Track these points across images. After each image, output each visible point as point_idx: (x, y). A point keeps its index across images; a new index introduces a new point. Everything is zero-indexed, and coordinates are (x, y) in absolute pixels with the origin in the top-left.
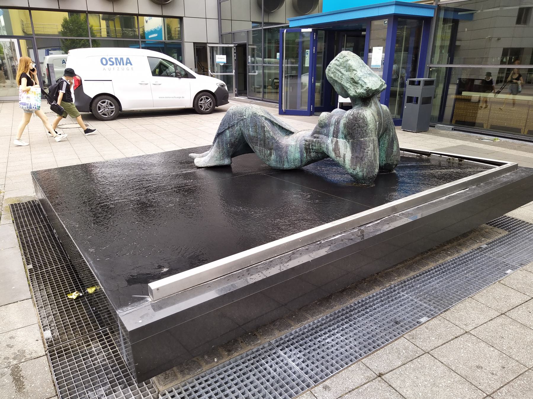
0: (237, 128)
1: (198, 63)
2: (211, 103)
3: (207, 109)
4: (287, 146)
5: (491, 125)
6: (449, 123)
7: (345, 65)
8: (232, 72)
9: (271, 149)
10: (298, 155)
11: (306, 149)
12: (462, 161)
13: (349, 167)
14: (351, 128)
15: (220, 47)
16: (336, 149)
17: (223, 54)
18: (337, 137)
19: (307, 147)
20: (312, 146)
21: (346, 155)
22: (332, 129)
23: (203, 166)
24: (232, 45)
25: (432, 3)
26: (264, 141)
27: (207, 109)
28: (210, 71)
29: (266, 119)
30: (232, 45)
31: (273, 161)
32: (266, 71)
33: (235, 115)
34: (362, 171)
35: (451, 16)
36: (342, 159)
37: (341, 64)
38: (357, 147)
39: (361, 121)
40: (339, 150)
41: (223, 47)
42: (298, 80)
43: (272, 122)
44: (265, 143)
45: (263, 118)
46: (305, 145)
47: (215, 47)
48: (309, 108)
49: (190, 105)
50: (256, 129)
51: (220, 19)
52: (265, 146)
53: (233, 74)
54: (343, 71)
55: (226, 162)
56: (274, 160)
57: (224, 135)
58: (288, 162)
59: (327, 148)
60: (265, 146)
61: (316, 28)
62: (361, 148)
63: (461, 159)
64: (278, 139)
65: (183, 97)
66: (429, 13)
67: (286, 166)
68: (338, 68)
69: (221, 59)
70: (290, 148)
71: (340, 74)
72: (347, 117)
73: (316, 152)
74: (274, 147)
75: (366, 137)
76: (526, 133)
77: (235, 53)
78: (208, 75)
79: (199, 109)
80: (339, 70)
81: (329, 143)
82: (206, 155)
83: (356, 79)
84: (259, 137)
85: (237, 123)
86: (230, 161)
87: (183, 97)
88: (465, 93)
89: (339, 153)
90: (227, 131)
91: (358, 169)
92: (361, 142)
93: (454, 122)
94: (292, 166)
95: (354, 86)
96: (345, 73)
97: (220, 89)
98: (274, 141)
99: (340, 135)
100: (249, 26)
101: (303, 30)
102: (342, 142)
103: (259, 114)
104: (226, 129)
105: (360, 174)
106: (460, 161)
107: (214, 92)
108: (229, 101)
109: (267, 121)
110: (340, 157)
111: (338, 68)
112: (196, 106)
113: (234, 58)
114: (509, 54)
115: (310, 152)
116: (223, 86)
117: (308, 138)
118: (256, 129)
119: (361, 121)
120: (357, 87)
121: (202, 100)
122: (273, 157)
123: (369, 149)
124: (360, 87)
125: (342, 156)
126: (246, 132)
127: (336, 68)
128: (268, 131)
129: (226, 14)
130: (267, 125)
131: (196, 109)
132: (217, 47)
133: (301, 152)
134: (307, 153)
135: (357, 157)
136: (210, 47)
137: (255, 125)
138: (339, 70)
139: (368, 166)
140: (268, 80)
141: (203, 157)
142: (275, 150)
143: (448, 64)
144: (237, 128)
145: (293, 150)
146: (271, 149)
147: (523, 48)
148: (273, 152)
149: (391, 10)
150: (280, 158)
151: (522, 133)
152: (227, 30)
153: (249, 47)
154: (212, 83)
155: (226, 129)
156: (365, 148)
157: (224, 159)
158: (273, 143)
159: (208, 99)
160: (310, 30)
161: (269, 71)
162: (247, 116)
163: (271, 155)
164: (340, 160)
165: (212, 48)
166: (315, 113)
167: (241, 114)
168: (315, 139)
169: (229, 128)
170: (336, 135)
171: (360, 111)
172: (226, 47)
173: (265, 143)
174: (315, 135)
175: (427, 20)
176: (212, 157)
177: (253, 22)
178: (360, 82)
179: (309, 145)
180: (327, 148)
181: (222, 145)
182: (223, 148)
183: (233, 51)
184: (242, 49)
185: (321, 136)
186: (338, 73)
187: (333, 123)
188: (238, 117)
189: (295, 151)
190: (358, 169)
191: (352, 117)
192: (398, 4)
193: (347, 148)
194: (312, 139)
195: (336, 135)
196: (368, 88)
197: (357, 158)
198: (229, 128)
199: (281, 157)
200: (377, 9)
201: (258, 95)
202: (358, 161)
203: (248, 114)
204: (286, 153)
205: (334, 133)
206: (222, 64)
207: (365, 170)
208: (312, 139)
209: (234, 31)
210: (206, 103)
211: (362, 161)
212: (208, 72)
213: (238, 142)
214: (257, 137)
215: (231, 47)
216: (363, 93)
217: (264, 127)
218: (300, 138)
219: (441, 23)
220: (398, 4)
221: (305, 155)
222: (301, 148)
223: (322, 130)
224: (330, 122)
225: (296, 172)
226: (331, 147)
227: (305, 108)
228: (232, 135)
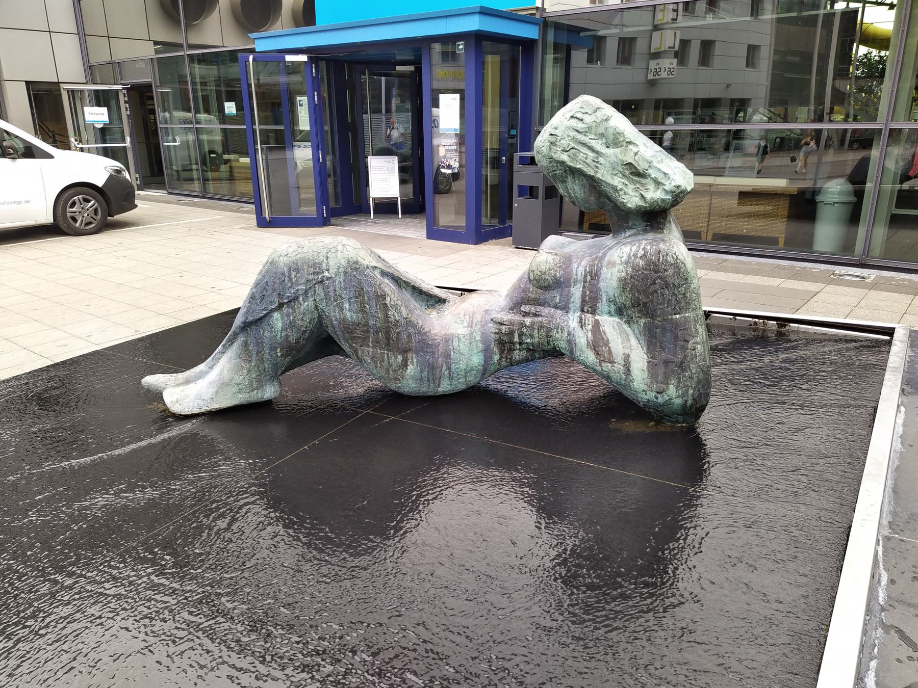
0: (306, 305)
1: (39, 120)
2: (96, 211)
3: (88, 224)
4: (447, 340)
5: (714, 234)
6: (576, 228)
7: (601, 130)
8: (124, 141)
9: (405, 352)
10: (477, 360)
11: (501, 343)
12: (785, 326)
13: (644, 387)
14: (645, 291)
15: (89, 91)
16: (598, 343)
17: (99, 105)
18: (593, 312)
19: (506, 339)
20: (520, 336)
21: (633, 358)
22: (577, 292)
23: (196, 411)
24: (119, 87)
25: (534, 14)
26: (387, 333)
27: (88, 224)
28: (72, 140)
29: (384, 274)
30: (119, 87)
31: (411, 379)
32: (204, 137)
33: (297, 270)
34: (685, 394)
35: (564, 39)
36: (619, 367)
37: (590, 128)
39: (671, 271)
40: (607, 344)
41: (96, 91)
42: (288, 153)
43: (397, 280)
44: (388, 339)
45: (377, 273)
46: (499, 333)
47: (77, 90)
48: (320, 211)
49: (46, 217)
50: (362, 304)
51: (82, 34)
52: (388, 344)
53: (128, 144)
54: (598, 145)
55: (269, 392)
56: (412, 377)
57: (264, 325)
58: (450, 377)
59: (571, 342)
60: (388, 344)
61: (316, 54)
62: (676, 338)
63: (783, 322)
64: (420, 323)
65: (27, 202)
66: (530, 32)
67: (445, 387)
68: (580, 137)
69: (97, 115)
70: (455, 344)
71: (591, 155)
72: (627, 263)
73: (529, 350)
74: (414, 344)
75: (687, 310)
76: (709, 238)
77: (126, 102)
78: (69, 148)
79: (69, 225)
80: (584, 145)
81: (572, 327)
82: (201, 376)
83: (641, 167)
84: (371, 322)
85: (306, 292)
86: (278, 388)
87: (27, 202)
89: (610, 352)
91: (672, 391)
92: (676, 324)
93: (586, 226)
94: (460, 385)
95: (634, 182)
96: (604, 150)
97: (114, 179)
98: (411, 330)
99: (603, 305)
100: (148, 51)
101: (289, 58)
102: (610, 325)
103: (366, 263)
104: (273, 311)
105: (678, 401)
106: (780, 326)
107: (100, 186)
108: (137, 202)
109: (386, 281)
110: (612, 362)
111: (580, 137)
112: (60, 218)
113: (125, 113)
115: (511, 350)
116: (119, 172)
117: (506, 317)
118: (362, 304)
119: (671, 271)
120: (643, 185)
121: (74, 204)
122: (411, 369)
123: (698, 339)
124: (651, 186)
125: (619, 359)
126: (333, 314)
127: (574, 139)
128: (396, 306)
129: (95, 25)
130: (388, 287)
131: (63, 226)
132: (81, 91)
133: (487, 352)
134: (501, 352)
135: (666, 362)
136: (68, 91)
137: (360, 293)
138: (584, 145)
139: (699, 382)
140: (255, 161)
141: (187, 382)
142: (417, 352)
144: (306, 305)
145: (463, 348)
146: (405, 352)
147: (683, 99)
148: (413, 358)
150: (431, 371)
151: (703, 238)
152: (100, 55)
153: (157, 91)
154: (97, 169)
155: (273, 311)
156: (688, 338)
157: (261, 386)
158: (409, 336)
159: (89, 201)
160: (303, 58)
161: (211, 138)
162: (333, 271)
163: (406, 365)
165: (72, 92)
166: (333, 220)
167: (316, 268)
168: (528, 321)
169: (281, 306)
170: (590, 305)
171: (662, 246)
172: (104, 91)
173: (388, 339)
174: (524, 308)
175: (528, 45)
176: (223, 385)
177: (156, 43)
178: (653, 173)
179: (511, 333)
180: (569, 342)
181: (258, 352)
182: (262, 360)
183: (122, 99)
184: (141, 95)
185: (545, 311)
186: (584, 150)
187: (580, 277)
188: (306, 274)
189: (471, 349)
190: (672, 391)
191: (641, 263)
193: (628, 340)
194: (517, 318)
195: (590, 305)
196: (678, 187)
198: (281, 306)
199: (432, 368)
201: (187, 186)
202: (673, 372)
203: (335, 263)
204: (447, 356)
205: (584, 302)
206: (100, 126)
207: (691, 392)
208: (517, 318)
209: (117, 58)
210: (84, 210)
211: (684, 370)
212: (69, 142)
213: (307, 340)
214: (366, 325)
215: (117, 91)
216: (663, 200)
217: (384, 297)
218: (478, 317)
219: (550, 50)
220: (485, 12)
221: (496, 357)
222: (485, 340)
223: (548, 295)
224: (570, 274)
225: (476, 399)
226: (582, 338)
227: (310, 210)
228: (292, 325)
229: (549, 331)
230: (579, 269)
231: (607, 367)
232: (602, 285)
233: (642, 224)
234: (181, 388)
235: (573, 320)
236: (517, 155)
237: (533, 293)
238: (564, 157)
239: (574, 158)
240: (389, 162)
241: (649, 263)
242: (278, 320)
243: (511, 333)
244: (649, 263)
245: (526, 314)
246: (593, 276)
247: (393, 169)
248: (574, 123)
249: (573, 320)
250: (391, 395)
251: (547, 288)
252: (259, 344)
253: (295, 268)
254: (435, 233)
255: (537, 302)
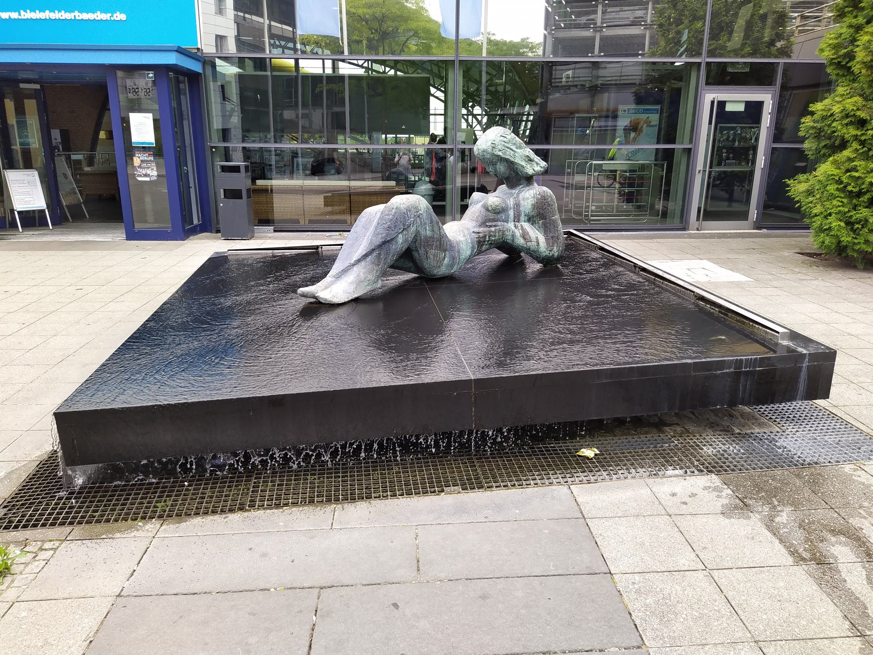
9: (445, 251)
16: (525, 235)
22: (511, 213)
23: (346, 300)
36: (534, 243)
38: (548, 228)
54: (513, 148)
59: (513, 236)
88: (260, 182)
90: (400, 236)
99: (522, 218)
102: (527, 226)
105: (556, 254)
114: (367, 130)
126: (423, 233)
143: (658, 143)
144: (413, 229)
149: (171, 59)
164: (532, 245)
168: (493, 229)
176: (359, 283)
179: (485, 236)
185: (499, 223)
190: (555, 249)
192: (180, 51)
195: (517, 219)
197: (551, 239)
200: (138, 54)
204: (459, 252)
220: (180, 51)
222: (472, 243)
228: (406, 240)
229: (504, 232)
230: (511, 202)
231: (529, 244)
232: (521, 209)
233: (525, 182)
234: (329, 289)
235: (511, 225)
236: (87, 169)
237: (491, 216)
238: (500, 153)
239: (505, 153)
240: (29, 175)
241: (542, 196)
242: (400, 239)
243: (485, 236)
244: (542, 196)
245: (491, 226)
246: (517, 205)
247: (35, 181)
248: (502, 138)
249: (511, 225)
250: (390, 292)
251: (498, 213)
252: (387, 254)
253: (408, 210)
254: (133, 235)
255: (494, 220)
